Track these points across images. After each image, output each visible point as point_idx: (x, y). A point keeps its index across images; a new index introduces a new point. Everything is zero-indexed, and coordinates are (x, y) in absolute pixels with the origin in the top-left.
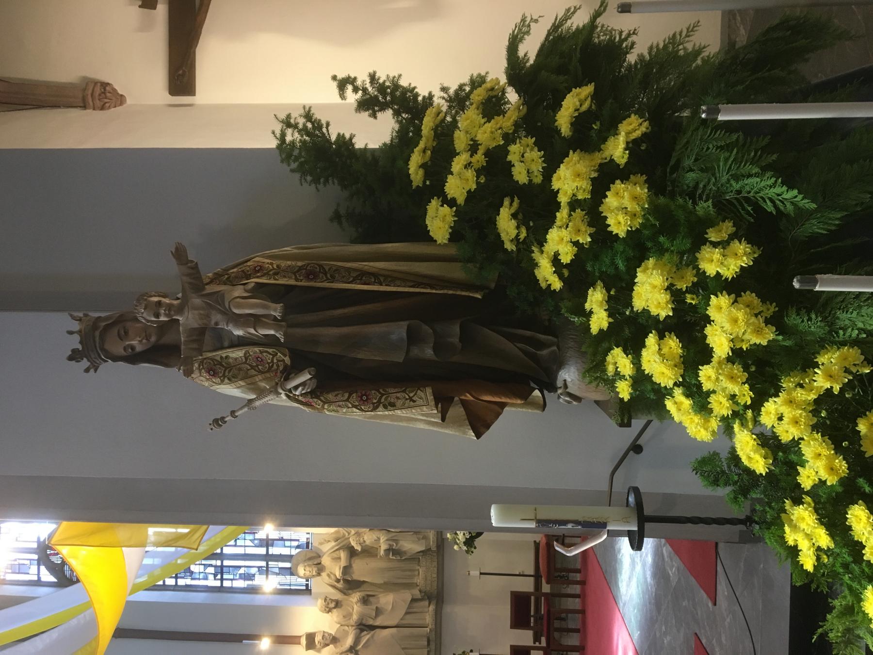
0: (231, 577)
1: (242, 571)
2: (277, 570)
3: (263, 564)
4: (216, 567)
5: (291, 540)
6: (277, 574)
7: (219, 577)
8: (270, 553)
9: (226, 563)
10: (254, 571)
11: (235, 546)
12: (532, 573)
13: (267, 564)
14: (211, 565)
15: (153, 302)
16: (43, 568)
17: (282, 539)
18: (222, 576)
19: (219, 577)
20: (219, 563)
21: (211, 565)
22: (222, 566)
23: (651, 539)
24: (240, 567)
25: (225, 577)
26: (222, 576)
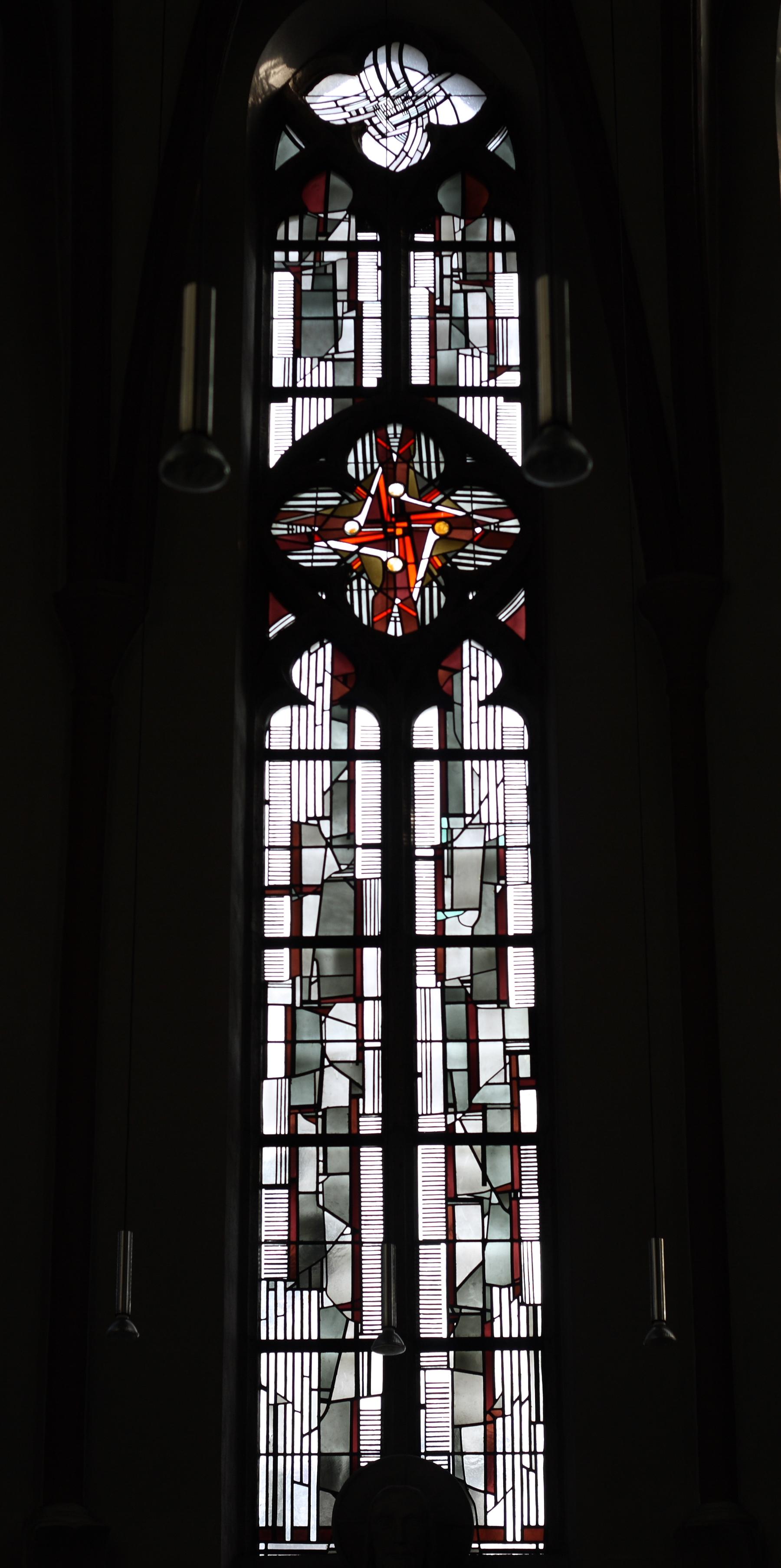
0: (307, 1183)
1: (334, 1227)
2: (344, 1388)
3: (373, 1322)
4: (353, 1112)
5: (490, 1453)
6: (325, 1390)
7: (305, 1127)
8: (426, 1358)
9: (372, 1160)
10: (340, 1287)
11: (452, 1199)
12: (441, 1039)
13: (369, 1346)
14: (357, 1091)
15: (674, 1334)
16: (318, 412)
17: (492, 1412)
18: (308, 1140)
19: (305, 1127)
20: (370, 1126)
21: (357, 1091)
22: (355, 1141)
23: (374, 950)
24: (354, 1221)
25: (308, 1154)
26: (308, 1140)
